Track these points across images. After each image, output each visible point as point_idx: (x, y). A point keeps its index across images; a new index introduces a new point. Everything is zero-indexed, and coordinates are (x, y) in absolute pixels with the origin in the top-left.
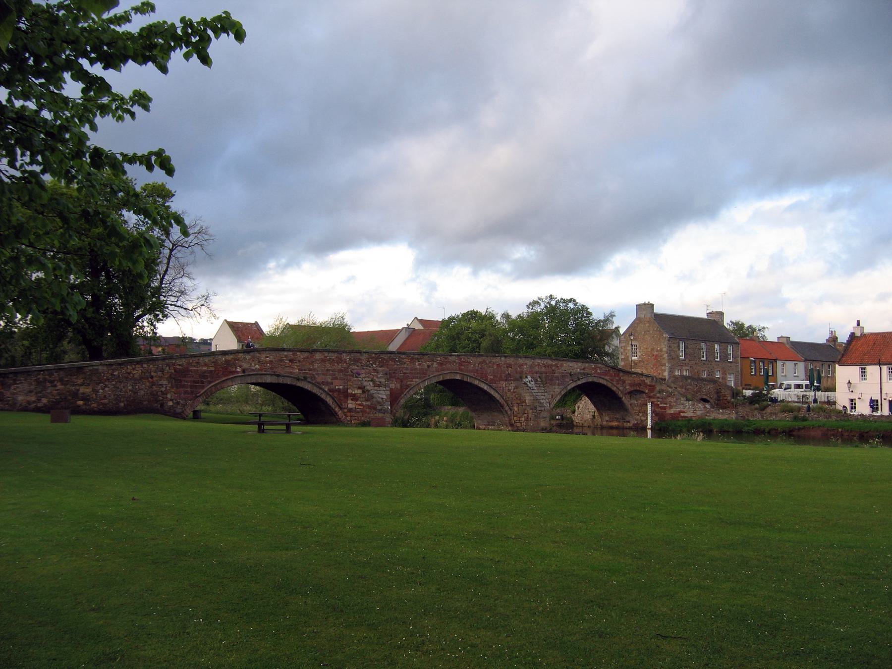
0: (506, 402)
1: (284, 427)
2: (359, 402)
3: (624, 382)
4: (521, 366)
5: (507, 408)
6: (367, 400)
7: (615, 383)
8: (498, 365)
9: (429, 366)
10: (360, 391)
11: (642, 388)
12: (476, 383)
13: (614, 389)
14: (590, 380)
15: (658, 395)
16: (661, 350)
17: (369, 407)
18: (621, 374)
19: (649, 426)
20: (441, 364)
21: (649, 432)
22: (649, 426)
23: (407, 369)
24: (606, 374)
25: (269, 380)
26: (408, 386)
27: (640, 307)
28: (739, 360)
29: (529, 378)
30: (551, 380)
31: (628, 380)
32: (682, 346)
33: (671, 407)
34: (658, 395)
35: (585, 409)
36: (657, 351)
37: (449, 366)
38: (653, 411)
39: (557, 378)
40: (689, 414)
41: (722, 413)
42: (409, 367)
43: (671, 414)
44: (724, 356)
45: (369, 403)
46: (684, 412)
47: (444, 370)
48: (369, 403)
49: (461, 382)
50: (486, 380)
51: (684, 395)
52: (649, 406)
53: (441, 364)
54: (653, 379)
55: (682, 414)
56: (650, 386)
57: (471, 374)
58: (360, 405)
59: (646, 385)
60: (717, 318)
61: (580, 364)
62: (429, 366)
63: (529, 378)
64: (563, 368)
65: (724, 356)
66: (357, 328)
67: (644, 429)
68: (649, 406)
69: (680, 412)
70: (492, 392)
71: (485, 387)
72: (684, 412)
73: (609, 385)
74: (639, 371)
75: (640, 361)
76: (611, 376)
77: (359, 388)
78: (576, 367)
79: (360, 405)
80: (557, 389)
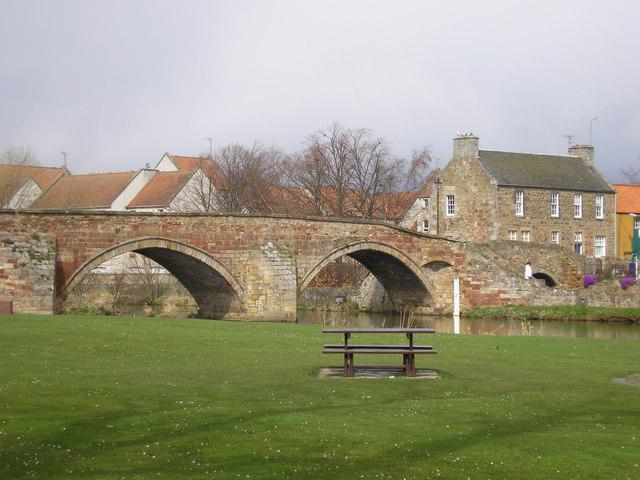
0: (236, 278)
1: (359, 360)
2: (8, 281)
3: (419, 250)
4: (257, 229)
5: (237, 287)
6: (20, 278)
7: (405, 251)
8: (223, 229)
9: (117, 231)
10: (11, 266)
11: (446, 258)
12: (189, 252)
13: (404, 259)
14: (365, 247)
15: (469, 268)
16: (487, 204)
17: (24, 288)
18: (415, 239)
19: (456, 312)
20: (136, 227)
21: (457, 320)
22: (456, 312)
23: (84, 234)
24: (389, 239)
25: (146, 245)
26: (85, 258)
27: (461, 140)
28: (615, 216)
29: (270, 244)
30: (305, 247)
31: (426, 247)
32: (521, 198)
33: (487, 285)
34: (469, 268)
35: (368, 287)
36: (482, 205)
37: (148, 229)
38: (463, 291)
39: (314, 245)
40: (512, 295)
41: (557, 295)
42: (87, 231)
43: (487, 295)
44: (590, 212)
45: (23, 282)
46: (504, 292)
47: (141, 235)
48: (23, 282)
49: (370, 252)
50: (205, 248)
51: (505, 269)
52: (457, 283)
53: (136, 227)
54: (461, 246)
55: (502, 296)
56: (457, 255)
57: (183, 241)
58: (9, 284)
59: (452, 254)
60: (583, 154)
61: (349, 226)
62: (117, 231)
63: (270, 244)
64: (323, 231)
65: (590, 212)
66: (78, 170)
67: (450, 315)
68: (457, 283)
69: (500, 292)
70: (214, 265)
71: (204, 259)
72: (504, 292)
73: (396, 254)
74: (455, 235)
75: (458, 220)
76: (399, 241)
77: (9, 261)
78: (344, 230)
79: (9, 284)
80: (314, 261)
